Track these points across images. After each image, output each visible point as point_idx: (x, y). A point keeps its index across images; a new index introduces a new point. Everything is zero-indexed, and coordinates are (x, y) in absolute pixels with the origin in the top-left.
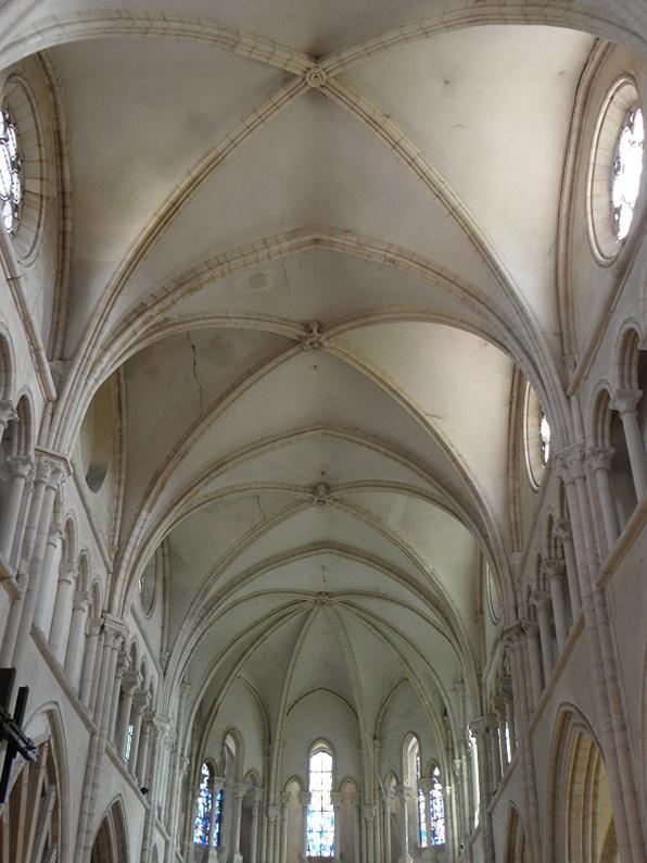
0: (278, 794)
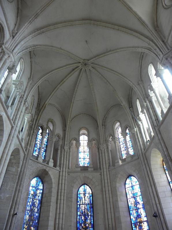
0: (68, 143)
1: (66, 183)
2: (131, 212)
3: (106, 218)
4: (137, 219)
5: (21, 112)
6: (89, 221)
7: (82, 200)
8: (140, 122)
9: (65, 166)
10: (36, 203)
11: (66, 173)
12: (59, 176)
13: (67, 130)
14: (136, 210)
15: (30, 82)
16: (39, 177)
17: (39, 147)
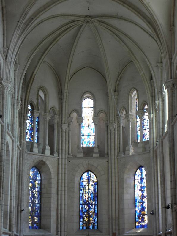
1: (66, 172)
2: (137, 204)
3: (110, 209)
6: (92, 210)
7: (85, 189)
9: (64, 152)
10: (35, 195)
11: (67, 160)
12: (58, 164)
13: (64, 100)
14: (142, 203)
16: (35, 167)
17: (29, 127)
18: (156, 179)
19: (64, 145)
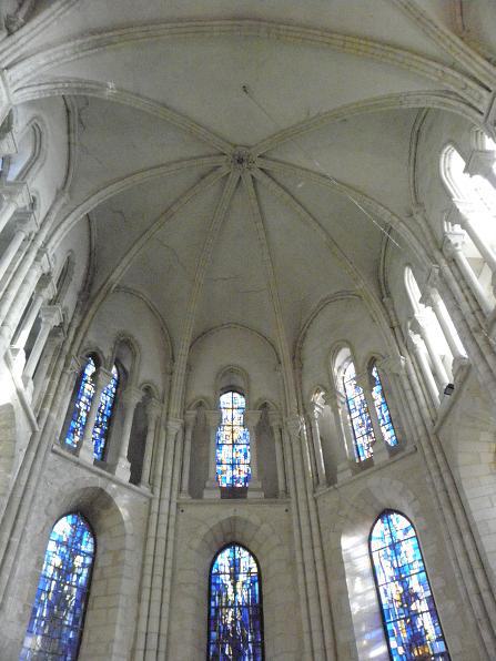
2: (390, 627)
4: (411, 651)
5: (25, 282)
8: (418, 336)
15: (63, 200)
18: (459, 512)
19: (170, 466)
